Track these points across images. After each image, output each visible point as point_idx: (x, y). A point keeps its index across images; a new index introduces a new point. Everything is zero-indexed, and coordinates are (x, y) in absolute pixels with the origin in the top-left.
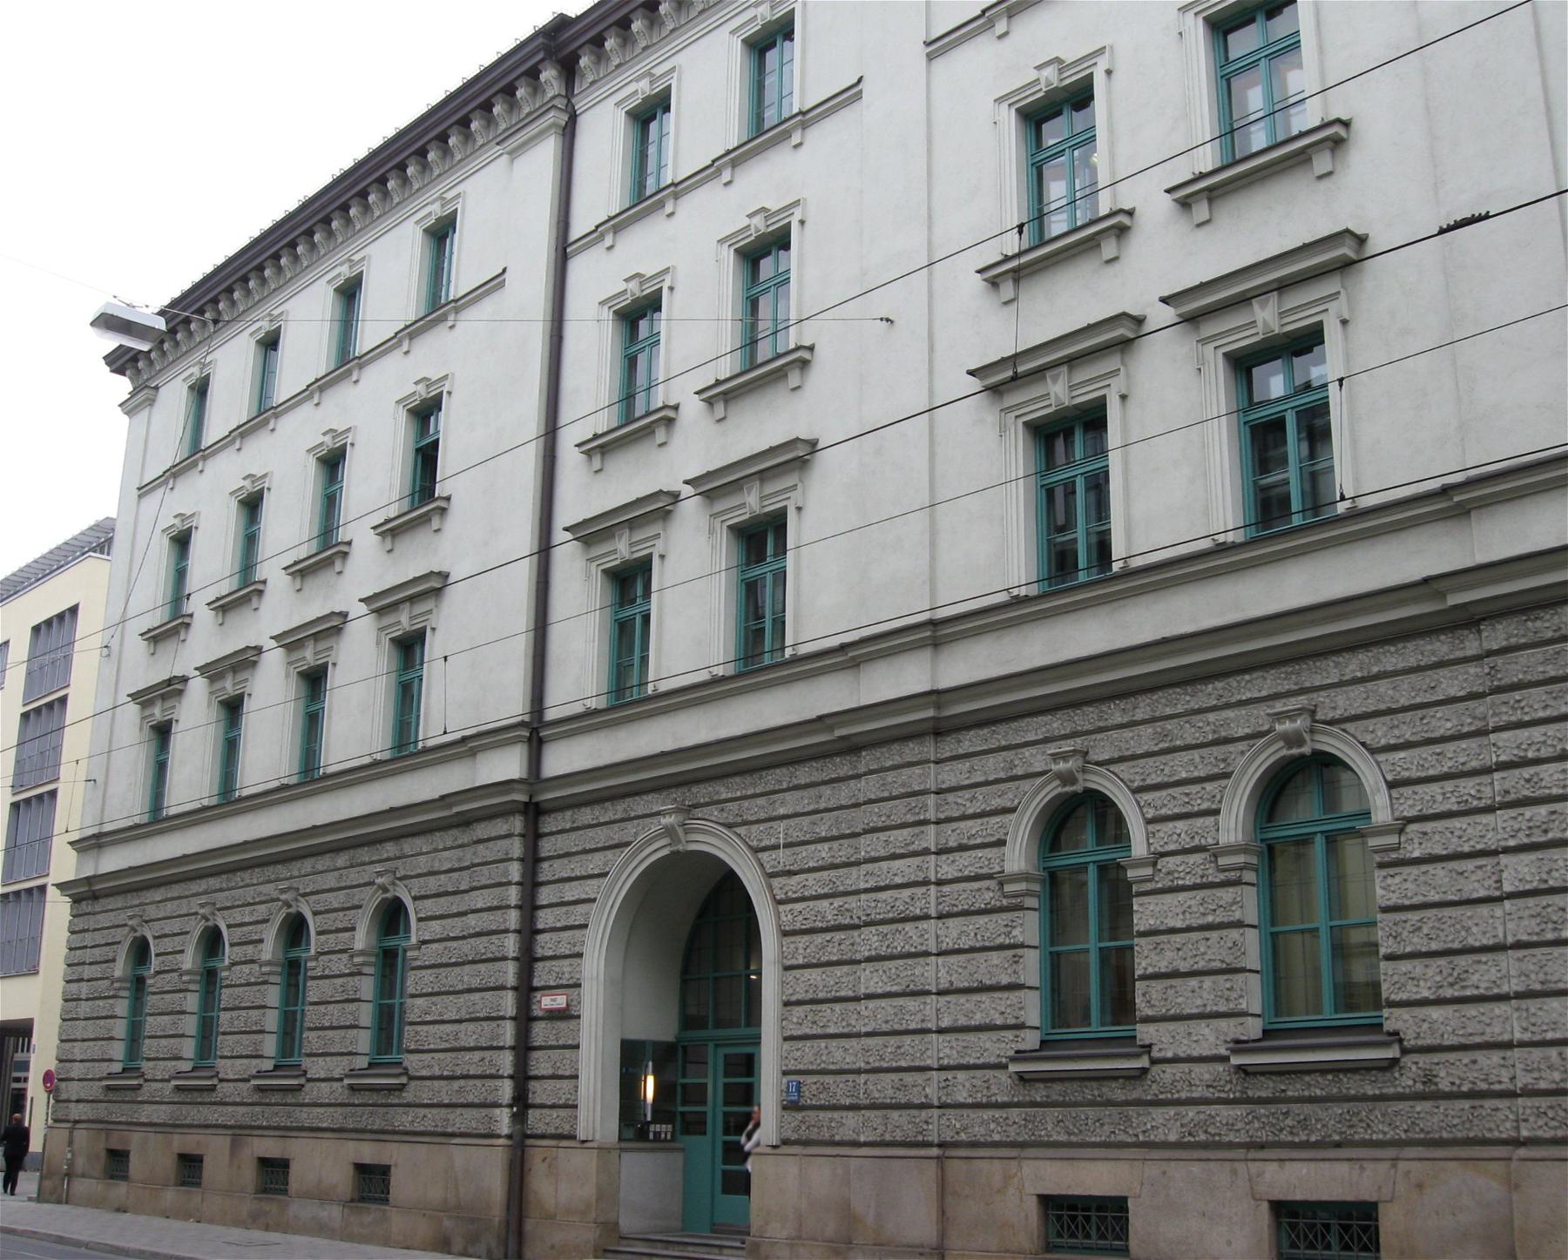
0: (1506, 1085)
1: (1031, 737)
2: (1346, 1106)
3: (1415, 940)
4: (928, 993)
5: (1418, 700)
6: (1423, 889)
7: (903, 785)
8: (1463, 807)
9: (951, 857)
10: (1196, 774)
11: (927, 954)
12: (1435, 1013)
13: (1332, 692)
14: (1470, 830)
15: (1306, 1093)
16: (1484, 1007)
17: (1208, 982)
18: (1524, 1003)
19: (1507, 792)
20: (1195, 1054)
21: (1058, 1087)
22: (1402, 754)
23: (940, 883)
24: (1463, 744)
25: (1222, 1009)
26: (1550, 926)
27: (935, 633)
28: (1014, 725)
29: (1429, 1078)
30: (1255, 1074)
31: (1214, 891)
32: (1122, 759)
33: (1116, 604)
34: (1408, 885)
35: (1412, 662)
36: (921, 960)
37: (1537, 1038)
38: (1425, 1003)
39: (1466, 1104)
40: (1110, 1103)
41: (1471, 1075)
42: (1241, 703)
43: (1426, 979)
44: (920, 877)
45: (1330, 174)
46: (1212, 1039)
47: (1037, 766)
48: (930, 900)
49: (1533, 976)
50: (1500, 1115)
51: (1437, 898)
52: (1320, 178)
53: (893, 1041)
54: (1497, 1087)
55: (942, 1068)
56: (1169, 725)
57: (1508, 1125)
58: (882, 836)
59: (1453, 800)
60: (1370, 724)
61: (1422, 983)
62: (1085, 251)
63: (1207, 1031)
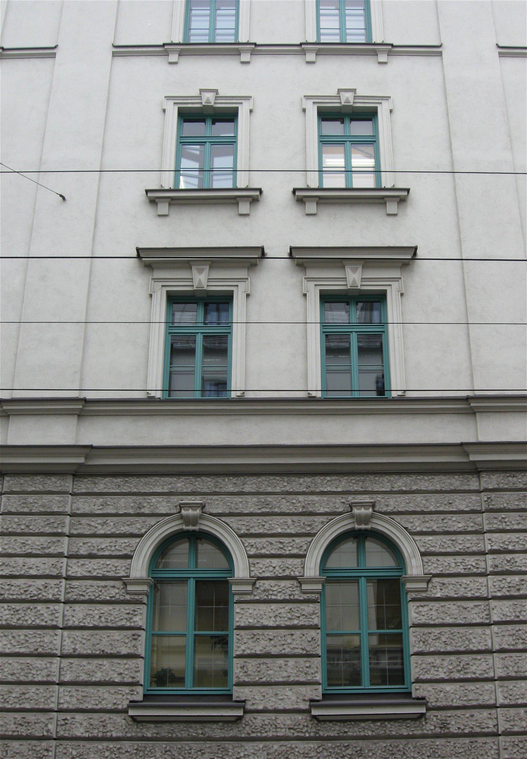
0: (492, 729)
1: (159, 490)
2: (389, 742)
3: (437, 644)
4: (54, 655)
5: (441, 509)
6: (442, 615)
7: (43, 506)
8: (467, 571)
9: (82, 561)
10: (288, 531)
11: (55, 627)
12: (448, 687)
13: (386, 496)
14: (471, 585)
15: (362, 734)
16: (478, 685)
17: (291, 662)
18: (506, 683)
19: (497, 566)
20: (280, 707)
21: (166, 727)
22: (431, 538)
23: (68, 578)
24: (469, 537)
25: (302, 679)
26: (521, 641)
27: (83, 408)
28: (143, 480)
29: (444, 725)
30: (325, 721)
31: (298, 605)
32: (231, 515)
33: (233, 417)
34: (433, 612)
35: (438, 487)
36: (51, 632)
37: (513, 702)
38: (442, 681)
39: (467, 740)
40: (210, 739)
41: (471, 724)
42: (322, 493)
43: (443, 667)
44: (55, 572)
45: (395, 215)
46: (294, 698)
47: (165, 507)
48: (59, 589)
49: (511, 668)
50: (488, 746)
51: (451, 621)
52: (389, 215)
53: (18, 689)
54: (486, 730)
55: (60, 711)
56: (269, 498)
57: (493, 752)
58: (20, 539)
59: (461, 567)
60: (411, 518)
61: (440, 669)
62: (223, 204)
63: (289, 693)
